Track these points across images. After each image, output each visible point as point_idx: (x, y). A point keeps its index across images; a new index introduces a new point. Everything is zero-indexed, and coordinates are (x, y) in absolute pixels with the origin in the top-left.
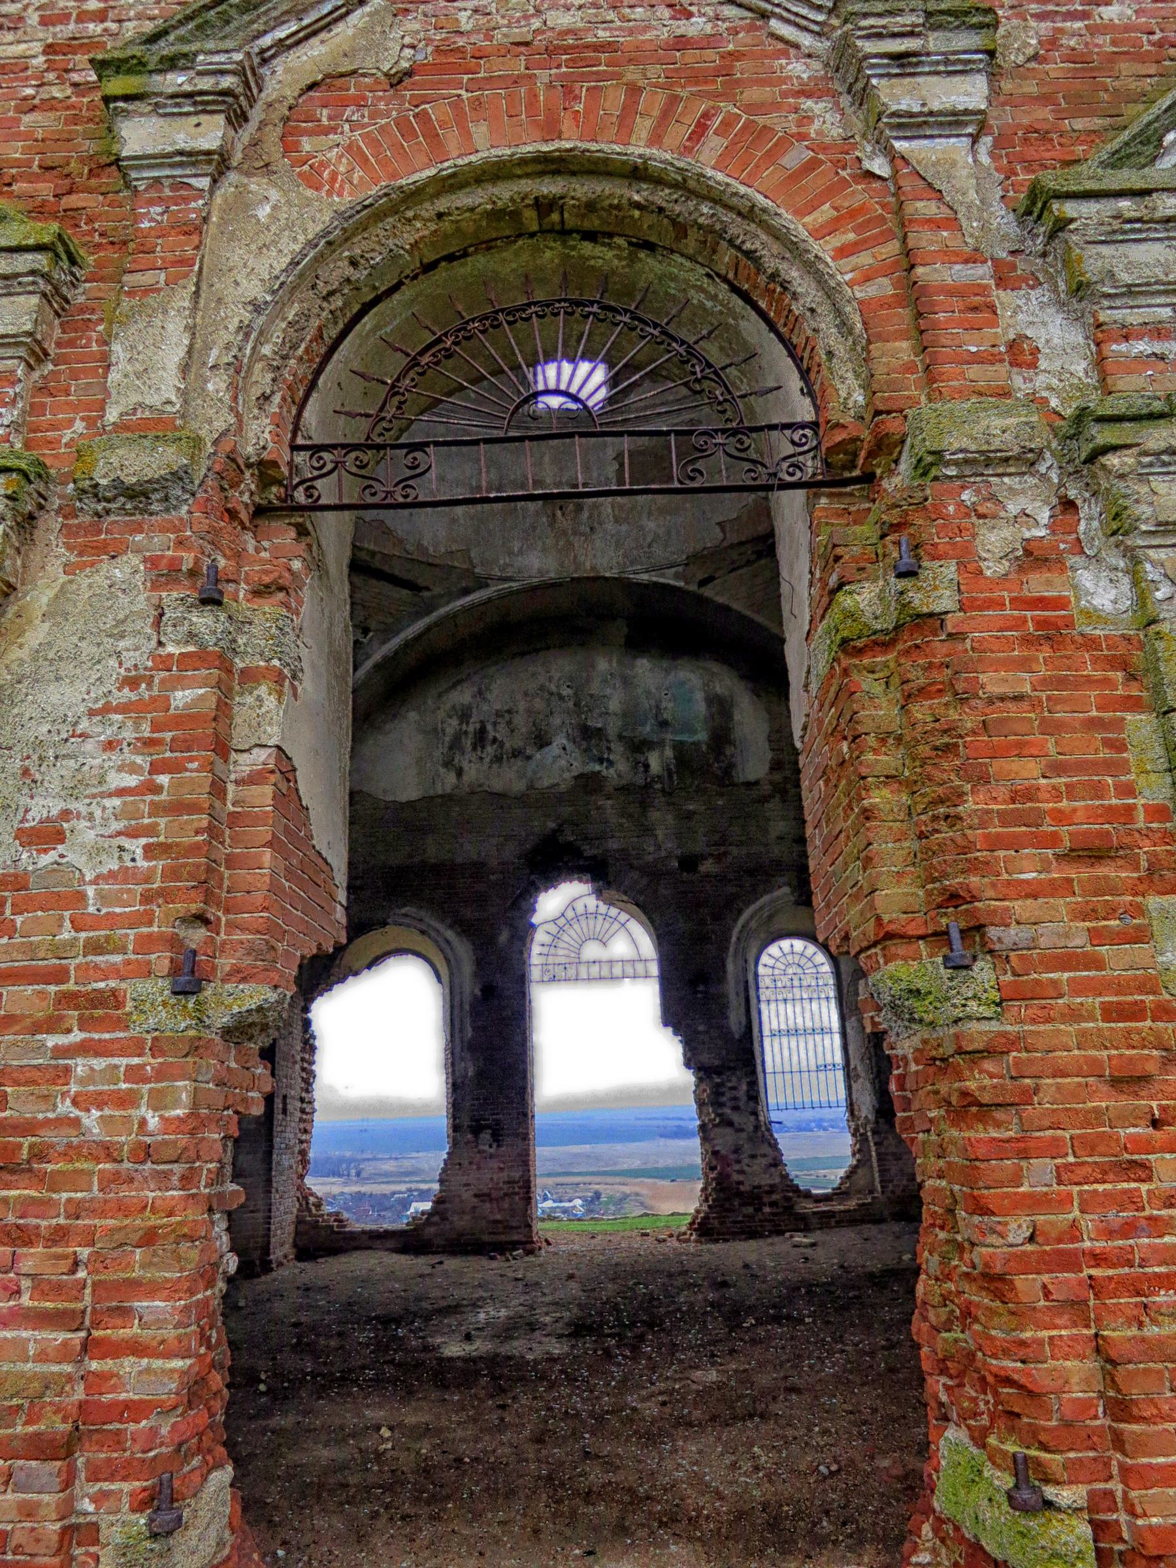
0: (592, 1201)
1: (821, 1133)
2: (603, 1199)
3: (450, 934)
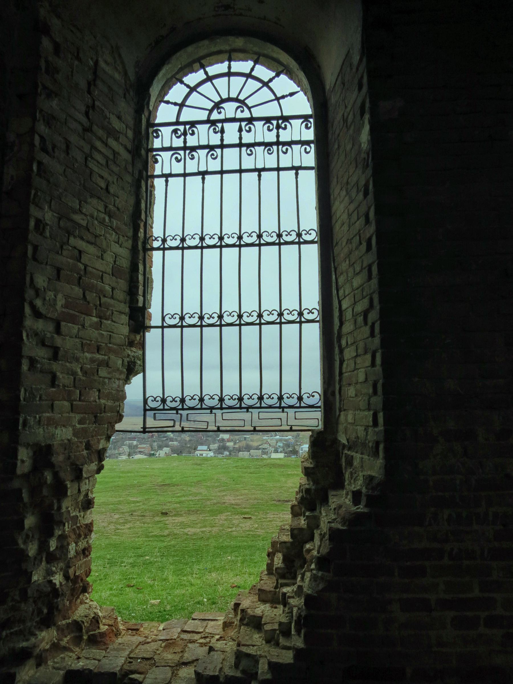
0: (296, 437)
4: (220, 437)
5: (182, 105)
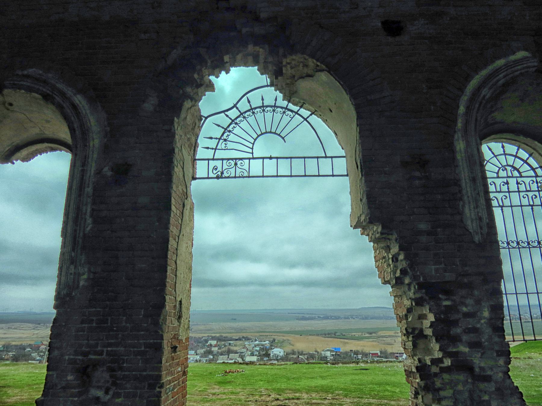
0: (272, 342)
1: (353, 320)
2: (276, 341)
3: (79, 100)
4: (209, 343)
5: (505, 154)
